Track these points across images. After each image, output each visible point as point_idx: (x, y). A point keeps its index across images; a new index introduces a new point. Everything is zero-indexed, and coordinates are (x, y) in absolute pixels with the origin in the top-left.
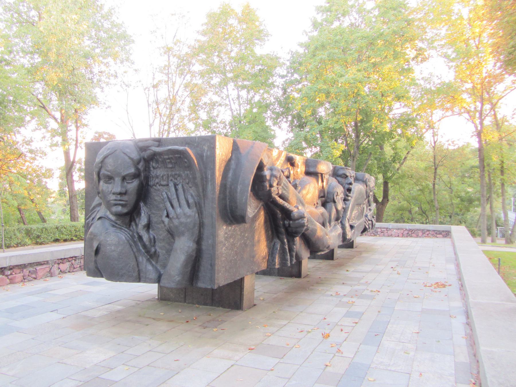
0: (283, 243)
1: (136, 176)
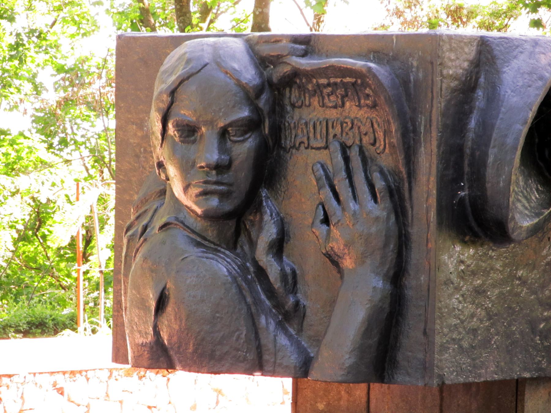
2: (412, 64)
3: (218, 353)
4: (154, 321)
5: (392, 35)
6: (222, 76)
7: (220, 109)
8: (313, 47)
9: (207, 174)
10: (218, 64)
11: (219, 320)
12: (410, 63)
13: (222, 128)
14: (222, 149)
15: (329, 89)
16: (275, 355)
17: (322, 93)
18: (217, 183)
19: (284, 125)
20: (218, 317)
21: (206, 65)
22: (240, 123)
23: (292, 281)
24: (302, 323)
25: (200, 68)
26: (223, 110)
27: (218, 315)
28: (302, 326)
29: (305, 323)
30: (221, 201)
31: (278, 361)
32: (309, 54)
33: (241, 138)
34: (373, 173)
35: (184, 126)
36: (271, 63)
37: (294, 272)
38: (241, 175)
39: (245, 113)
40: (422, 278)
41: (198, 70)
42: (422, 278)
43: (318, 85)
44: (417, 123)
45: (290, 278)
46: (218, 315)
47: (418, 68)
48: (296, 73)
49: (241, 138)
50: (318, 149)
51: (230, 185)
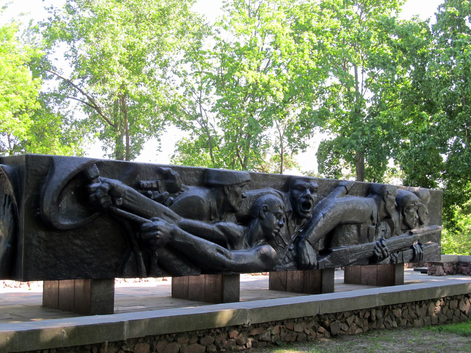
0: (136, 256)
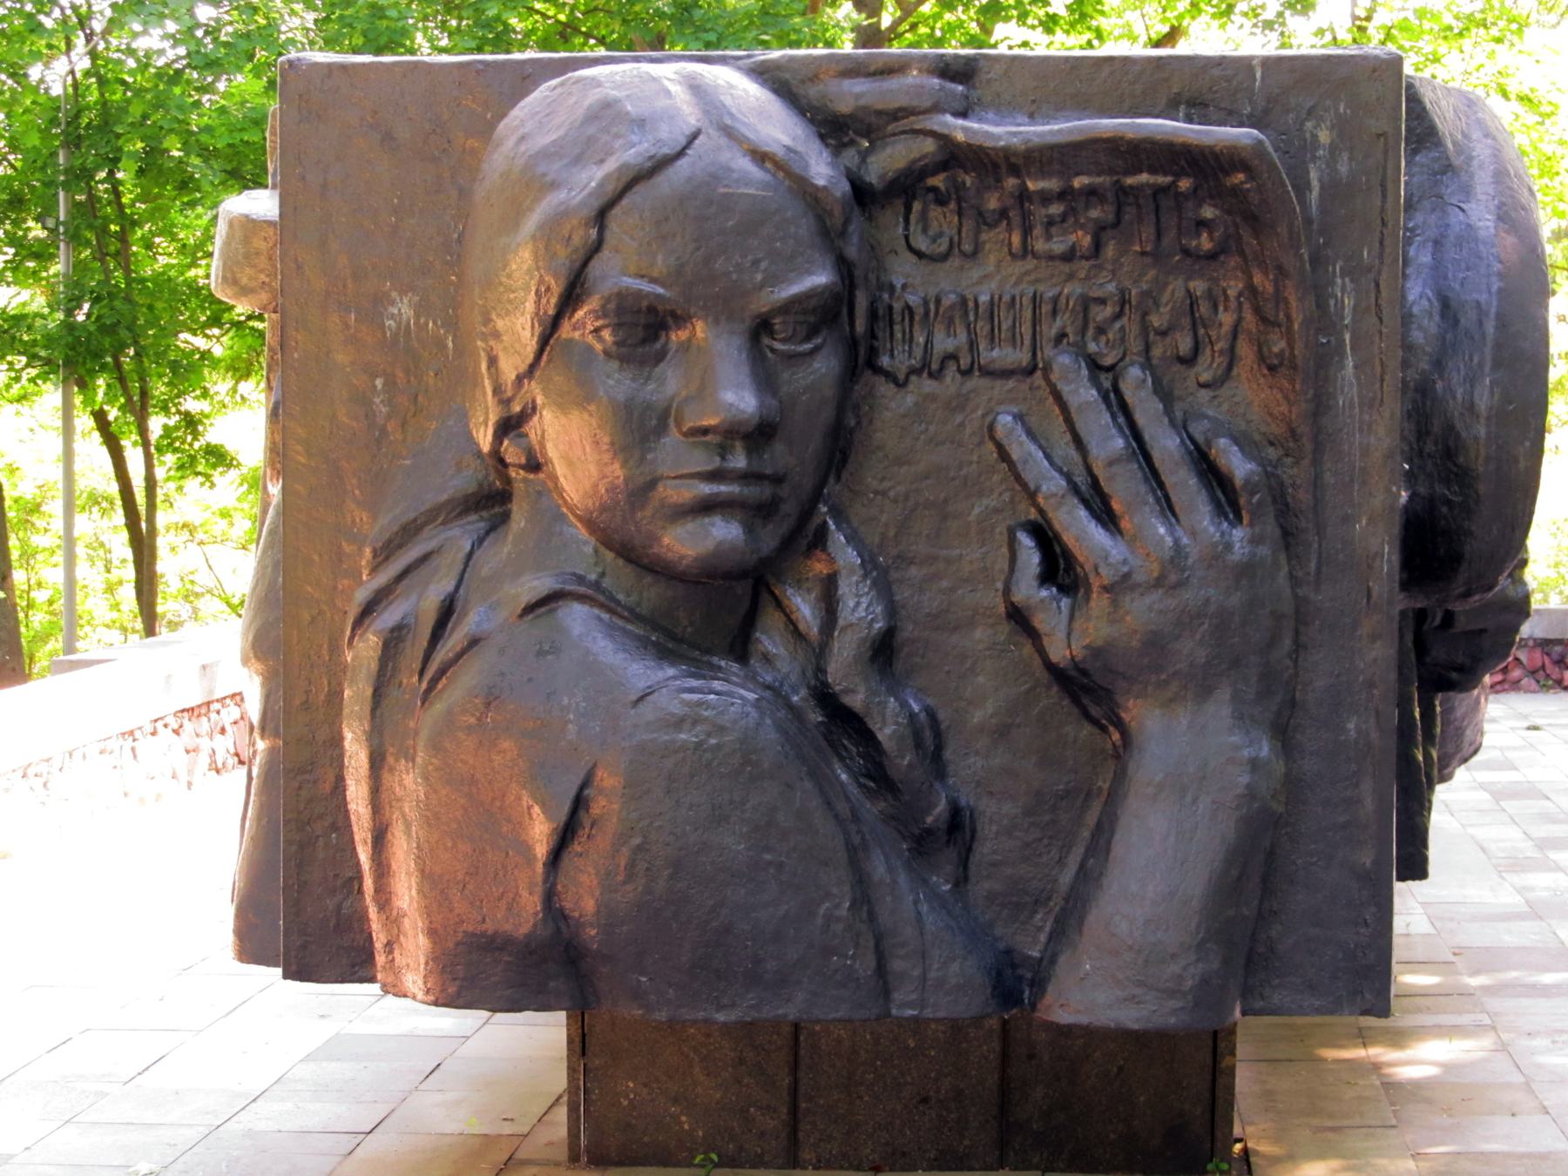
1: (824, 314)
2: (1314, 136)
3: (771, 965)
4: (545, 881)
5: (1251, 58)
6: (745, 164)
7: (756, 262)
8: (672, 118)
9: (723, 451)
10: (729, 132)
11: (772, 871)
12: (1308, 135)
13: (759, 316)
14: (765, 380)
15: (1056, 209)
16: (923, 955)
17: (1025, 215)
18: (714, 476)
19: (1319, 293)
20: (770, 863)
21: (694, 136)
22: (813, 302)
23: (931, 740)
24: (967, 858)
25: (683, 141)
26: (763, 265)
27: (768, 857)
28: (966, 867)
29: (975, 858)
30: (749, 529)
31: (933, 974)
32: (977, 109)
33: (808, 346)
34: (1128, 445)
35: (639, 311)
36: (868, 132)
37: (931, 714)
38: (791, 459)
39: (820, 278)
40: (1351, 726)
41: (679, 148)
42: (1351, 726)
43: (1023, 196)
44: (1332, 302)
45: (928, 734)
46: (768, 857)
47: (1333, 149)
48: (955, 156)
49: (808, 346)
50: (1006, 374)
51: (777, 480)
